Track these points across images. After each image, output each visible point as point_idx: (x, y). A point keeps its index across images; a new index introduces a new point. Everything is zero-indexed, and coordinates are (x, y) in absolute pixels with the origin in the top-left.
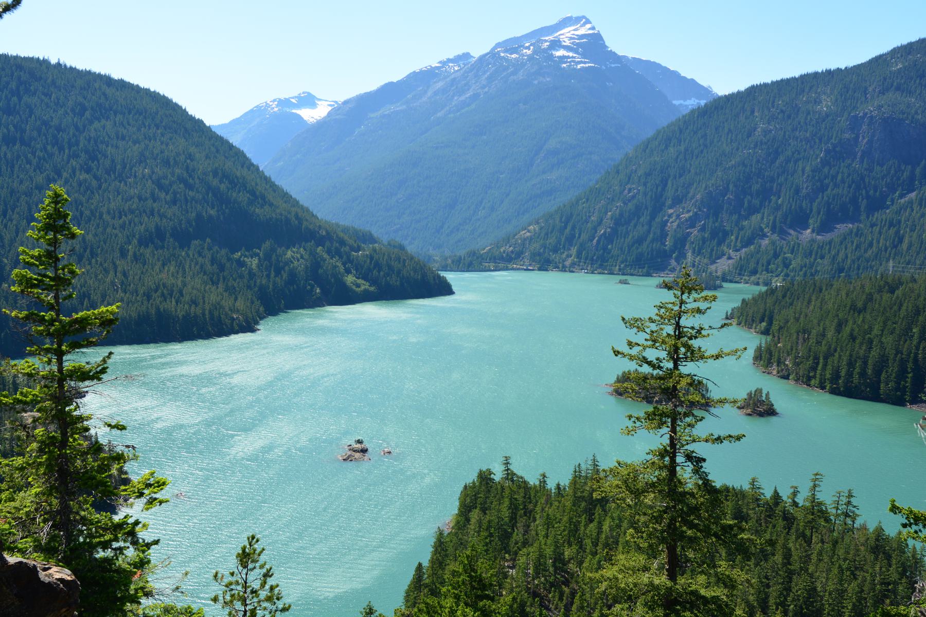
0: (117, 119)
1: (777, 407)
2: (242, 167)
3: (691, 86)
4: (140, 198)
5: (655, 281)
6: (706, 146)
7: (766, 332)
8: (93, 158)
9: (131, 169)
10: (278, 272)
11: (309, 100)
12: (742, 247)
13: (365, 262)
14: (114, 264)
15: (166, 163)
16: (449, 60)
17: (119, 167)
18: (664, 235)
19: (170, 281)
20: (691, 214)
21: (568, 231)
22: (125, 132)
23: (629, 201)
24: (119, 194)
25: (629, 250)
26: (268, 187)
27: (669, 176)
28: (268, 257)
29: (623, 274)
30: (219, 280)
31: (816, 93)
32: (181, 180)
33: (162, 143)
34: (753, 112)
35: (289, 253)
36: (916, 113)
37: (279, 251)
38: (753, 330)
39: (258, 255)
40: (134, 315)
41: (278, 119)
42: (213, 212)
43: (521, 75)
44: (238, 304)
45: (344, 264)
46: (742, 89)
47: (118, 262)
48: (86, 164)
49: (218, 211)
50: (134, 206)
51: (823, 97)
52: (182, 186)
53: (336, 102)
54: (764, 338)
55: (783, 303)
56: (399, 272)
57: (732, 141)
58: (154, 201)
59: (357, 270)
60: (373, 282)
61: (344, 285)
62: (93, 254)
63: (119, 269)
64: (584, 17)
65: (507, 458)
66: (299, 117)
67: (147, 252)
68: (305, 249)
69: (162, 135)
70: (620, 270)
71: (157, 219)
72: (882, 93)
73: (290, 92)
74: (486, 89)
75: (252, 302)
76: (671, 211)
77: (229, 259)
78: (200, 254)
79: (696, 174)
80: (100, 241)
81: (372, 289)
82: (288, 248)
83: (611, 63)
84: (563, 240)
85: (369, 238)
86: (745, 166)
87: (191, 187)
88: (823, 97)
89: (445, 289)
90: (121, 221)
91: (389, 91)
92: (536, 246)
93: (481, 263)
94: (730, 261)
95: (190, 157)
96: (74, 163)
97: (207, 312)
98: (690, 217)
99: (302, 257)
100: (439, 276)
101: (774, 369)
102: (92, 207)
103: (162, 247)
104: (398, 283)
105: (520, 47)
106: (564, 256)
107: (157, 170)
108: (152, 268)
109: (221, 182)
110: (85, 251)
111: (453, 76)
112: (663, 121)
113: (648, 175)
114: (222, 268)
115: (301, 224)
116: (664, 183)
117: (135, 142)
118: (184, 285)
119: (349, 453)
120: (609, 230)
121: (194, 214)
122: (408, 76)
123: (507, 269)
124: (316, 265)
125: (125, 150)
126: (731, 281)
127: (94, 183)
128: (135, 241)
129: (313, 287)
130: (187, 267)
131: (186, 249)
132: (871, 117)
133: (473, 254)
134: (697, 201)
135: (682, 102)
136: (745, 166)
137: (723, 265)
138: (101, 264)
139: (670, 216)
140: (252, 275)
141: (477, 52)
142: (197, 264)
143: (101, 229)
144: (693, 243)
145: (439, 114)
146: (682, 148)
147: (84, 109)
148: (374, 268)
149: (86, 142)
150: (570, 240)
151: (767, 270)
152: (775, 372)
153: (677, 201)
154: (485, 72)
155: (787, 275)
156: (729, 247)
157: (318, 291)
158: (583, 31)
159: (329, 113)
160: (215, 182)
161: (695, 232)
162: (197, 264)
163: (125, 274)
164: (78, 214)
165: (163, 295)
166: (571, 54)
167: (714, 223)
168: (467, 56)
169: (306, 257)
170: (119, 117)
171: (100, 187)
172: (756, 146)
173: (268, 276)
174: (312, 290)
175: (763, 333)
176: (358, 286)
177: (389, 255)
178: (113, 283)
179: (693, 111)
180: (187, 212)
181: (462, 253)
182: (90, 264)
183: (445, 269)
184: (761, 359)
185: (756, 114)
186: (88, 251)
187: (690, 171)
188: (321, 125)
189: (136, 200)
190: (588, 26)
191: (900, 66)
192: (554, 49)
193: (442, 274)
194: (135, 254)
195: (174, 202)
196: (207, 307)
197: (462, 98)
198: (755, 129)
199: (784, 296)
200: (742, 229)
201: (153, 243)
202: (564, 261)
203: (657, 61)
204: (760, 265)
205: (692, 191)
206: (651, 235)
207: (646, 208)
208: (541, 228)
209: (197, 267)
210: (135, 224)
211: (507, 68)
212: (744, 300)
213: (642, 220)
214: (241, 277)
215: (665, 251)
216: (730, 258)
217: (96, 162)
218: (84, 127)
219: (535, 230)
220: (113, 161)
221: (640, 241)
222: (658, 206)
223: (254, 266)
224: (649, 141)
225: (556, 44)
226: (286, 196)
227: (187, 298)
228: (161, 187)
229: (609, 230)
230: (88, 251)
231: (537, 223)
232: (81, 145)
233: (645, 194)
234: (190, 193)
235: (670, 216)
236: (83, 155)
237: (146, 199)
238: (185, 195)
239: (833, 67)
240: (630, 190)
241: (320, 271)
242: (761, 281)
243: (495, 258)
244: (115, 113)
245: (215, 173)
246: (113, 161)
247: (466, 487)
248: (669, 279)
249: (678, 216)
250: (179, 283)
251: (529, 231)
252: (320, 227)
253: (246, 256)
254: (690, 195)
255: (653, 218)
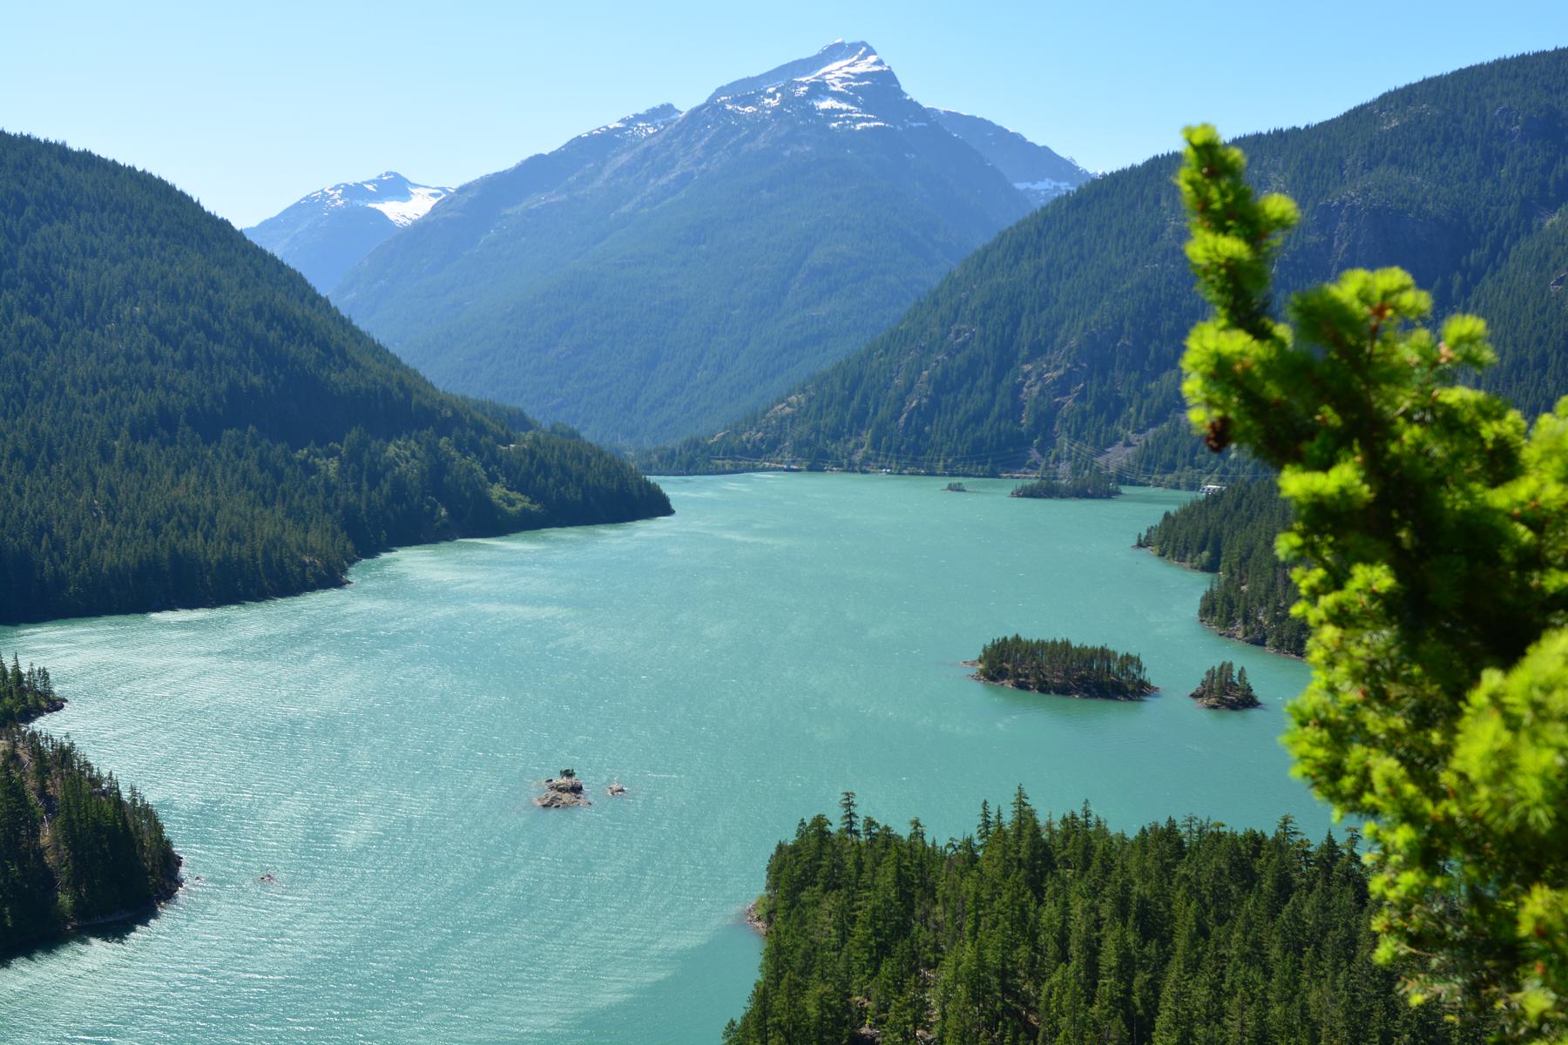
0: (82, 221)
1: (1258, 692)
2: (302, 301)
3: (1044, 160)
4: (129, 357)
5: (1009, 484)
6: (1082, 258)
7: (1211, 567)
8: (43, 289)
9: (110, 307)
10: (374, 483)
11: (396, 187)
12: (1150, 425)
13: (521, 461)
14: (91, 472)
15: (172, 295)
16: (638, 117)
17: (88, 303)
18: (1018, 408)
19: (192, 502)
20: (1061, 372)
21: (855, 403)
22: (96, 242)
23: (958, 351)
24: (90, 351)
25: (961, 432)
26: (347, 335)
27: (1023, 308)
28: (355, 456)
29: (952, 475)
30: (274, 498)
31: (1260, 168)
32: (201, 325)
33: (163, 261)
34: (1157, 200)
35: (391, 450)
36: (1425, 200)
37: (375, 445)
38: (1187, 564)
39: (337, 453)
40: (132, 561)
41: (348, 215)
42: (257, 380)
43: (761, 142)
44: (310, 538)
45: (486, 466)
46: (1139, 162)
47: (97, 470)
48: (29, 299)
49: (266, 378)
50: (120, 372)
51: (1273, 175)
52: (201, 335)
53: (443, 189)
54: (1208, 576)
55: (1236, 519)
56: (580, 478)
57: (1124, 248)
58: (154, 363)
59: (508, 476)
60: (537, 496)
61: (488, 501)
62: (53, 457)
63: (101, 481)
64: (864, 44)
65: (848, 795)
66: (381, 215)
67: (148, 451)
68: (418, 442)
69: (163, 248)
70: (946, 467)
71: (160, 393)
72: (1369, 166)
73: (364, 172)
74: (703, 166)
75: (334, 536)
76: (1027, 367)
77: (290, 461)
78: (239, 454)
79: (1067, 304)
80: (62, 434)
81: (535, 508)
82: (388, 440)
83: (912, 120)
84: (848, 418)
85: (520, 421)
86: (1150, 291)
87: (216, 337)
88: (1273, 175)
89: (658, 506)
90: (97, 398)
91: (536, 170)
92: (802, 430)
93: (709, 461)
94: (1129, 450)
95: (213, 284)
96: (9, 298)
97: (259, 555)
98: (1060, 377)
99: (413, 456)
100: (647, 484)
101: (1239, 629)
102: (46, 374)
103: (173, 442)
104: (579, 497)
105: (758, 93)
106: (851, 445)
107: (157, 307)
108: (159, 479)
109: (269, 327)
110: (39, 452)
111: (646, 145)
112: (1006, 219)
113: (987, 307)
114: (279, 476)
115: (408, 397)
116: (1015, 320)
117: (115, 260)
118: (217, 508)
119: (552, 794)
120: (925, 401)
121: (224, 385)
122: (569, 145)
123: (755, 470)
124: (439, 468)
125: (99, 275)
126: (1133, 483)
127: (47, 332)
128: (124, 433)
129: (434, 506)
130: (218, 476)
131: (214, 445)
132: (1353, 207)
133: (694, 444)
134: (1070, 350)
135: (1029, 185)
136: (1150, 291)
137: (1117, 457)
138: (68, 474)
139: (1026, 376)
140: (330, 489)
141: (687, 100)
142: (234, 471)
143: (62, 413)
144: (1066, 420)
145: (625, 209)
146: (1043, 261)
147: (23, 202)
148: (538, 472)
149: (29, 261)
150: (860, 419)
151: (1192, 463)
152: (1240, 634)
153: (1038, 350)
154: (700, 138)
155: (1225, 471)
156: (1126, 425)
157: (443, 512)
158: (862, 68)
159: (434, 208)
160: (259, 328)
161: (1069, 402)
162: (234, 471)
163: (112, 491)
164: (21, 387)
165: (180, 525)
166: (845, 106)
167: (1099, 386)
168: (668, 109)
169: (421, 454)
170: (85, 217)
171: (57, 340)
172: (1165, 256)
173: (358, 489)
174: (433, 512)
175: (1205, 569)
176: (511, 503)
177: (561, 449)
178: (90, 507)
179: (1058, 201)
180: (212, 381)
181: (674, 443)
182: (48, 473)
183: (649, 469)
184: (1213, 614)
185: (1164, 204)
186: (43, 452)
187: (1057, 301)
188: (422, 228)
189: (122, 360)
190: (872, 59)
191: (1395, 123)
192: (817, 98)
193: (652, 479)
194: (126, 454)
195: (189, 363)
196: (259, 545)
197: (663, 181)
198: (1163, 229)
199: (1238, 506)
200: (1147, 395)
201: (155, 435)
202: (851, 454)
203: (987, 118)
204: (1180, 455)
205: (1062, 333)
206: (997, 409)
207: (987, 363)
208: (810, 400)
209: (237, 476)
210: (122, 404)
211: (737, 130)
212: (1167, 515)
213: (979, 383)
214: (313, 490)
215: (1020, 434)
216: (1128, 444)
217: (47, 296)
218: (25, 233)
219: (799, 403)
220: (78, 293)
221: (978, 418)
222: (1006, 362)
223: (332, 472)
224: (987, 251)
225: (820, 89)
226: (378, 351)
227: (222, 530)
228: (164, 337)
229: (925, 401)
230: (43, 452)
231: (804, 391)
232: (21, 266)
233: (984, 339)
234: (216, 347)
235: (1026, 376)
236: (24, 283)
237: (139, 359)
238: (207, 351)
239: (1286, 125)
240: (958, 334)
241: (447, 479)
242: (1182, 480)
243: (733, 452)
244: (79, 209)
245: (258, 312)
246: (78, 293)
247: (780, 848)
248: (1032, 480)
249: (1040, 376)
250: (209, 506)
251: (789, 405)
252: (442, 403)
253: (317, 456)
254: (1059, 340)
255: (998, 379)
